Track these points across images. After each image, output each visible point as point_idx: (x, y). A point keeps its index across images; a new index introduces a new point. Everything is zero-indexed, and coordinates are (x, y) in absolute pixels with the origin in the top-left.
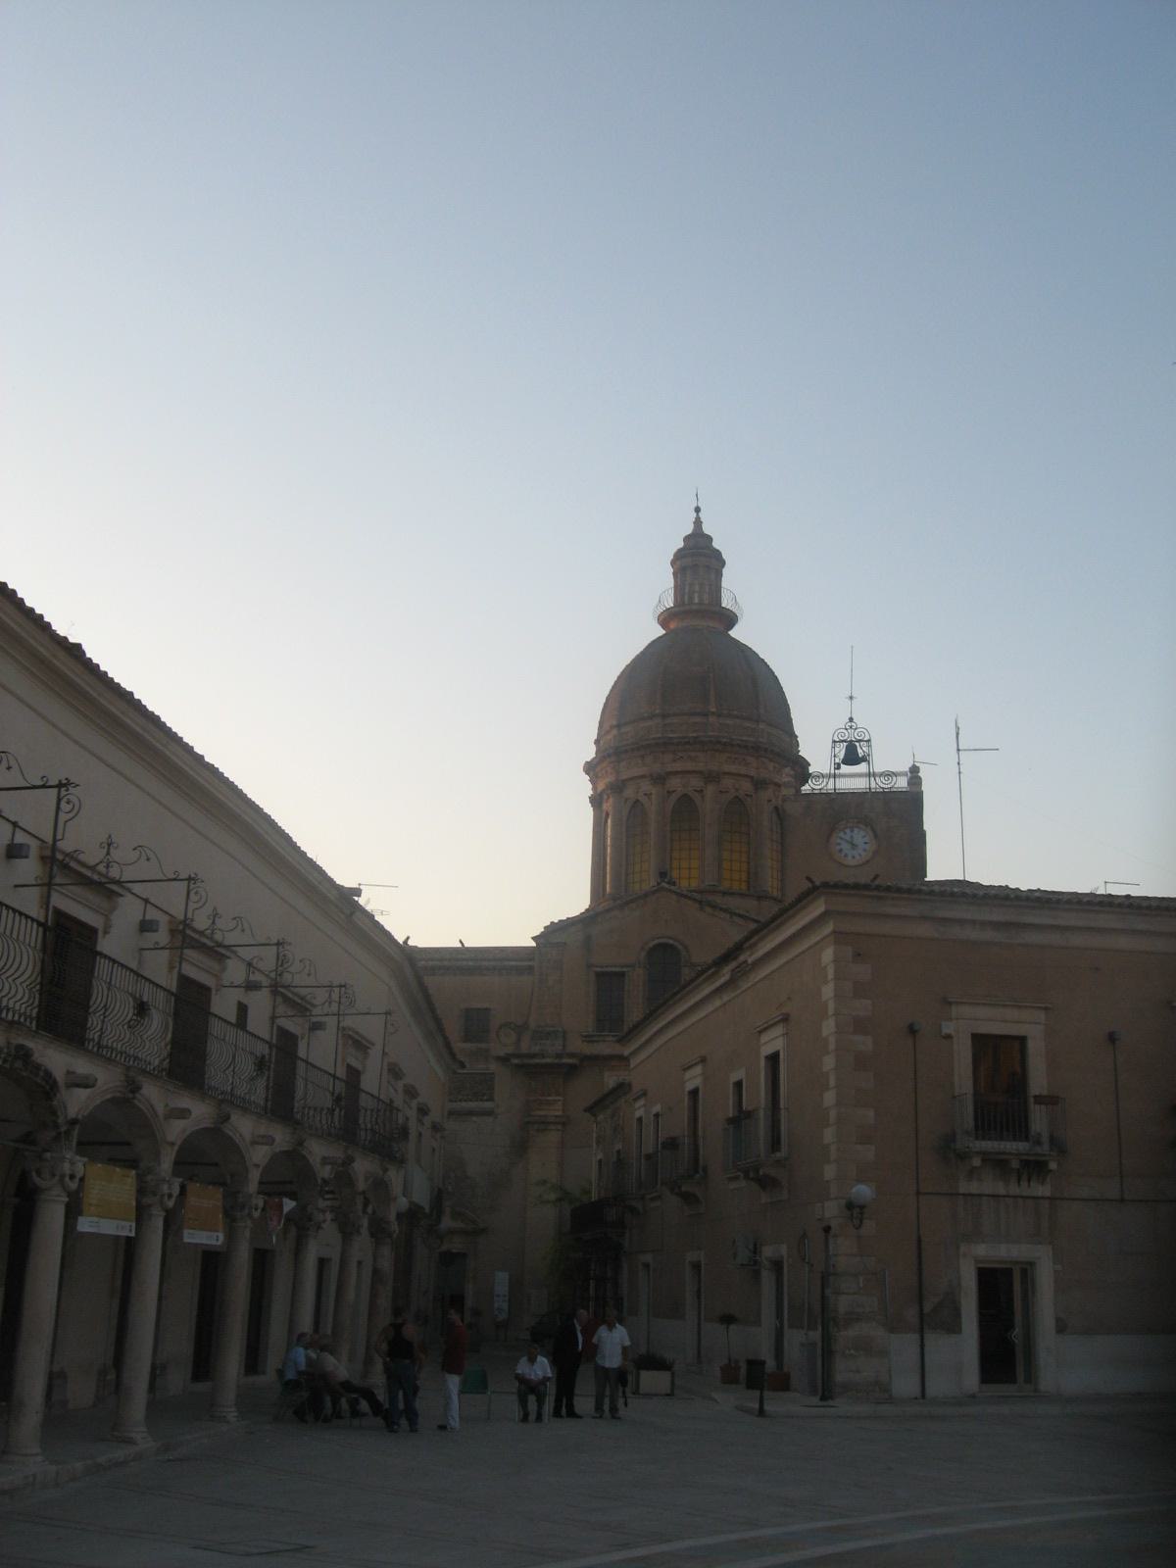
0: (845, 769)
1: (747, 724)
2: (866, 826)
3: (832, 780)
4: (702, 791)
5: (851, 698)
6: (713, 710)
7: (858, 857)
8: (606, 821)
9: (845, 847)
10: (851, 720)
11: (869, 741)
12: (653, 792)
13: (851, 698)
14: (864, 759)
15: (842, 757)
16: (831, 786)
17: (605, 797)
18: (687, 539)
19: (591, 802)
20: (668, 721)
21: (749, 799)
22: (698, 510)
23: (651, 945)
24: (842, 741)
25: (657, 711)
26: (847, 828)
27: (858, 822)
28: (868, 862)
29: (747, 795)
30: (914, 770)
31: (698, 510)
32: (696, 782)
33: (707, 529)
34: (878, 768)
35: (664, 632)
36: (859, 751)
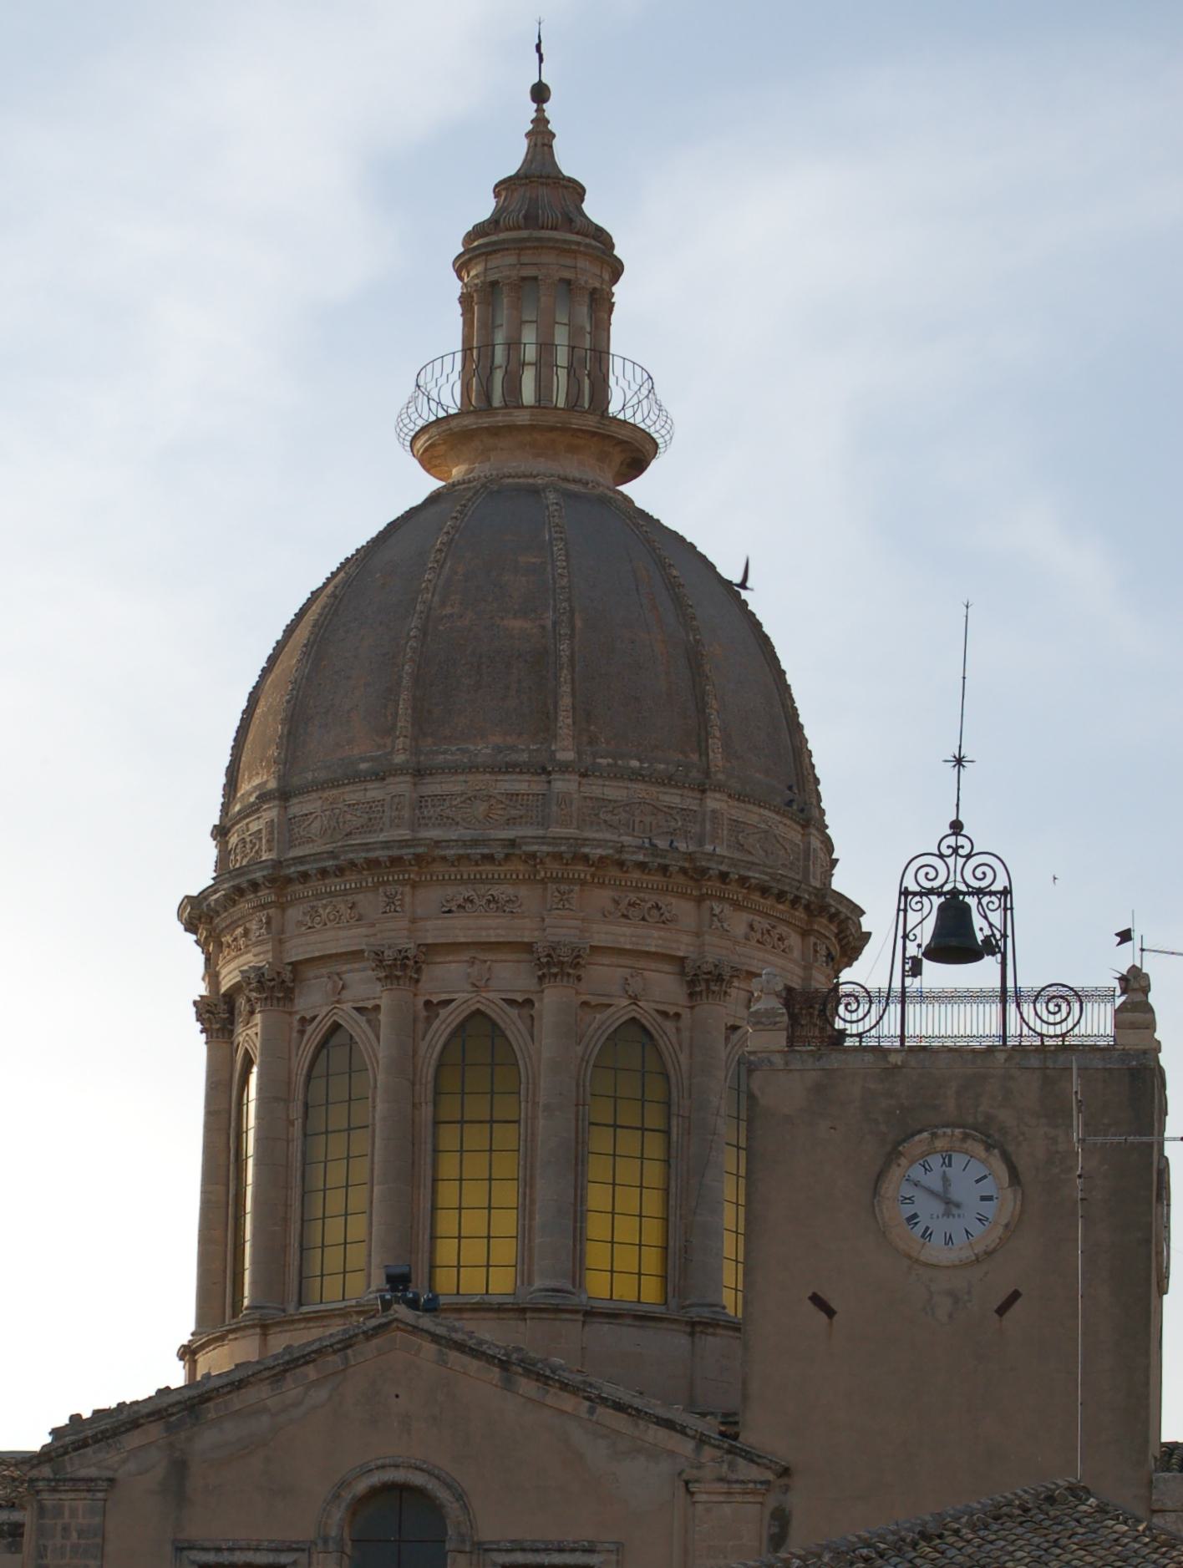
0: (937, 975)
1: (672, 798)
2: (988, 1147)
3: (894, 1009)
4: (529, 1003)
5: (959, 761)
6: (569, 756)
7: (959, 1238)
8: (244, 1082)
9: (927, 1208)
10: (957, 827)
11: (1006, 892)
12: (385, 1002)
13: (959, 761)
14: (990, 947)
15: (926, 941)
16: (890, 1026)
17: (241, 1002)
18: (504, 188)
19: (199, 1018)
20: (432, 787)
21: (669, 1026)
22: (540, 93)
23: (361, 1487)
24: (930, 892)
25: (399, 759)
26: (934, 1152)
27: (966, 1137)
28: (989, 1254)
29: (664, 1014)
30: (1134, 983)
31: (540, 93)
32: (512, 976)
33: (569, 162)
34: (1029, 978)
35: (433, 484)
36: (978, 922)
